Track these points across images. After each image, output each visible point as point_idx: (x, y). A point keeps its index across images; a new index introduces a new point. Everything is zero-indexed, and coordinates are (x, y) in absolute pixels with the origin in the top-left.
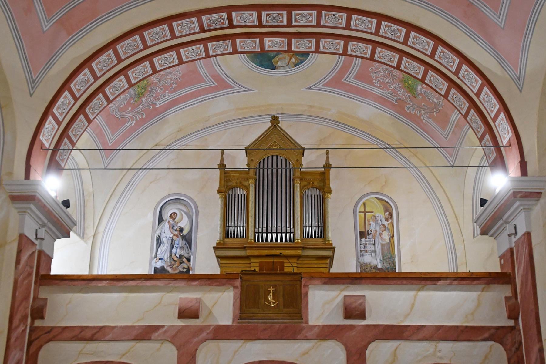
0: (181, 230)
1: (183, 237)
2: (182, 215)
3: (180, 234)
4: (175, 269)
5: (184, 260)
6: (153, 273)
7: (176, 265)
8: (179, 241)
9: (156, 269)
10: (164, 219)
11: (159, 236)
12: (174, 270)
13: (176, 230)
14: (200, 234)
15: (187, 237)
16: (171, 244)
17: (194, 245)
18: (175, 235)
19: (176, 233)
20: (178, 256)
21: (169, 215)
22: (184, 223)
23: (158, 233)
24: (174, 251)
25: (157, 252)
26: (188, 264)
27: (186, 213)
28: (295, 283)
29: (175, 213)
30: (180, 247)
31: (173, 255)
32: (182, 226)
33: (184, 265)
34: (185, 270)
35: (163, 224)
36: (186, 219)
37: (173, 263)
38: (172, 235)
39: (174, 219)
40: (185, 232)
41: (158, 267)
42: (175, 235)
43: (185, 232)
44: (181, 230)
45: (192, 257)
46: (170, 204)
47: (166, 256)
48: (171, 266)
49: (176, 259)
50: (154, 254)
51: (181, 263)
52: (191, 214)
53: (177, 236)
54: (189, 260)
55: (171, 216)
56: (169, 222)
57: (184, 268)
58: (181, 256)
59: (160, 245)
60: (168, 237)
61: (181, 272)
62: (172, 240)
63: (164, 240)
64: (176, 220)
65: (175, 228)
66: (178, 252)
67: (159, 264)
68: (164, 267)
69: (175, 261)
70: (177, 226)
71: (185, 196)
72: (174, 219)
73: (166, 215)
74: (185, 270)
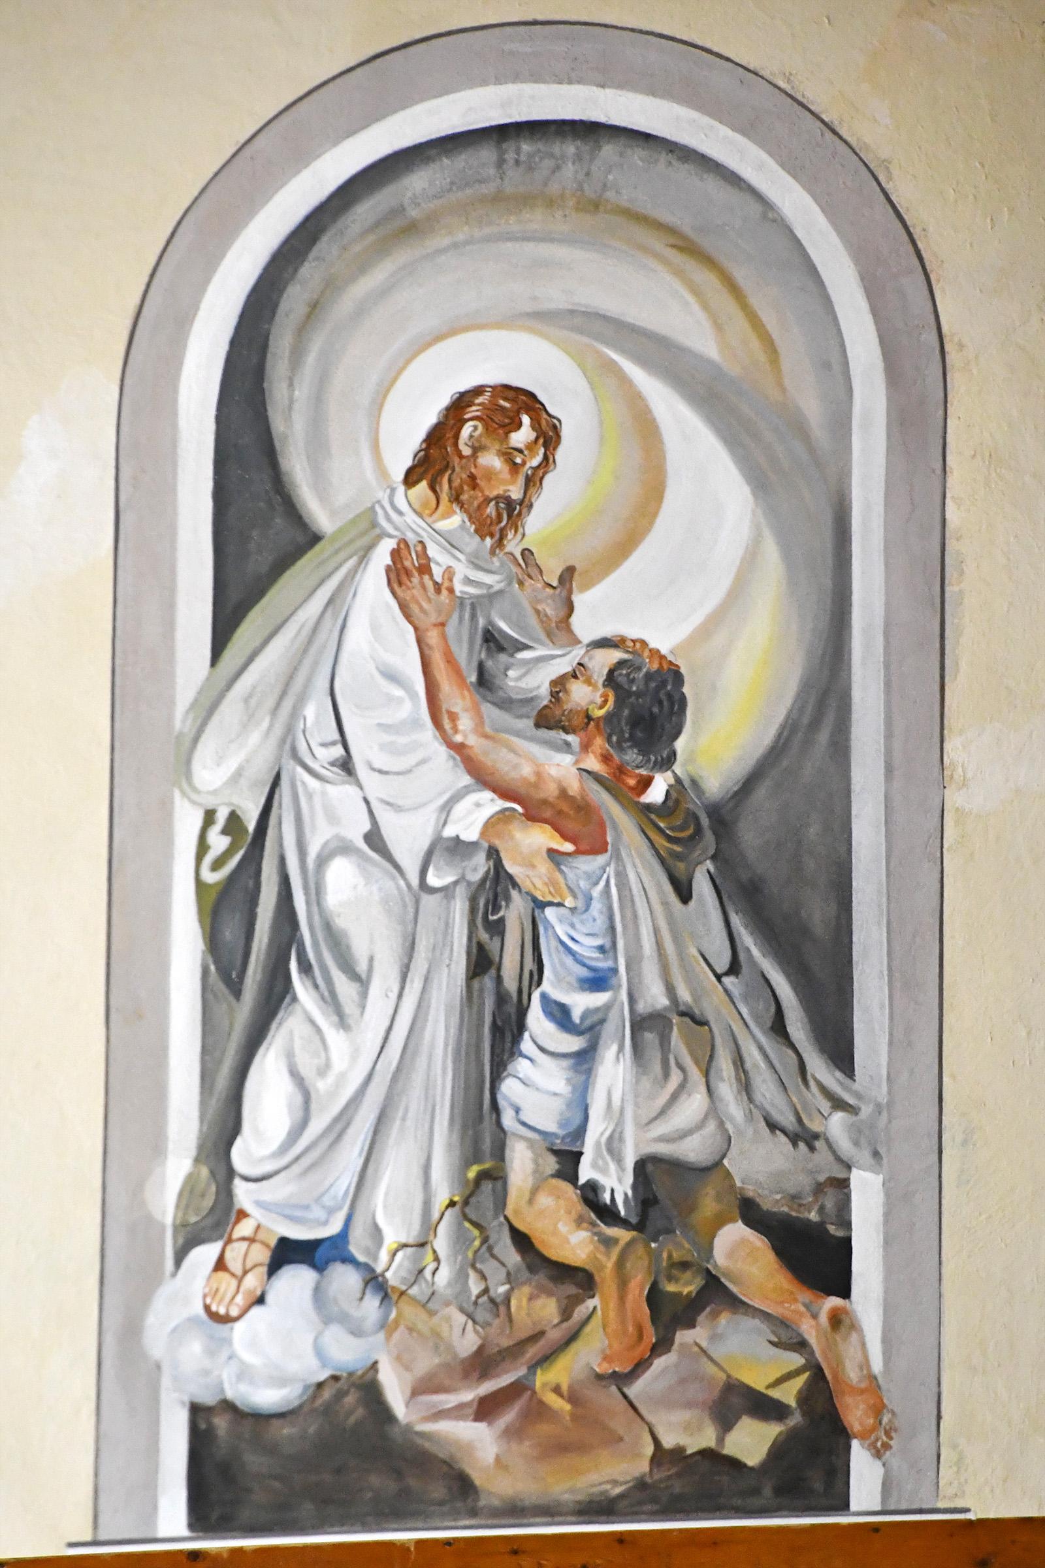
0: (646, 705)
1: (694, 835)
2: (645, 429)
3: (623, 785)
4: (583, 1432)
5: (737, 1249)
6: (171, 1522)
7: (589, 1354)
8: (617, 917)
9: (228, 1460)
10: (320, 514)
11: (253, 841)
12: (559, 1448)
13: (551, 718)
14: (982, 764)
15: (751, 836)
16: (481, 963)
17: (899, 979)
18: (531, 805)
19: (560, 765)
20: (618, 1186)
21: (403, 441)
22: (690, 580)
23: (225, 771)
24: (535, 1088)
25: (225, 1124)
26: (811, 1316)
27: (710, 393)
28: (669, 1483)
29: (514, 404)
30: (644, 1024)
31: (522, 1163)
32: (664, 637)
33: (742, 1351)
34: (751, 1442)
35: (293, 606)
36: (711, 491)
37: (539, 1309)
38: (474, 814)
39: (500, 519)
40: (717, 744)
41: (267, 1397)
42: (531, 805)
43: (717, 744)
44: (646, 705)
45: (867, 1195)
46: (405, 229)
47: (403, 1193)
48: (498, 1371)
49: (573, 1242)
50: (178, 1165)
51: (669, 1315)
52: (812, 407)
53: (576, 823)
54: (816, 1255)
55: (434, 461)
56: (405, 570)
57: (737, 1402)
58: (664, 1193)
59: (276, 995)
60: (409, 837)
61: (702, 1478)
62: (497, 885)
63: (348, 892)
64: (539, 523)
65: (533, 674)
66: (626, 1115)
67: (278, 1351)
68: (367, 1387)
69: (575, 1280)
70: (560, 628)
71: (687, 65)
72: (500, 519)
73: (356, 452)
74: (751, 1442)
